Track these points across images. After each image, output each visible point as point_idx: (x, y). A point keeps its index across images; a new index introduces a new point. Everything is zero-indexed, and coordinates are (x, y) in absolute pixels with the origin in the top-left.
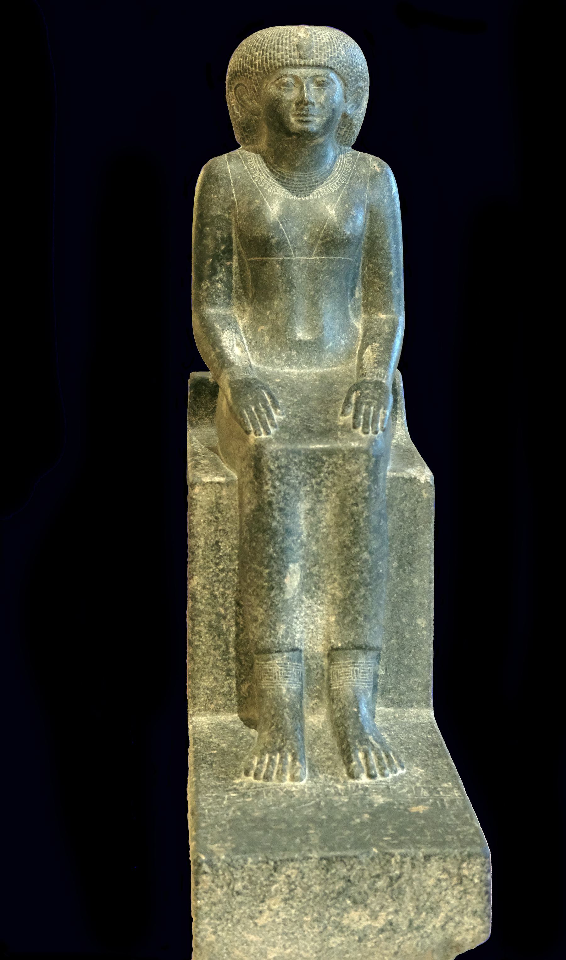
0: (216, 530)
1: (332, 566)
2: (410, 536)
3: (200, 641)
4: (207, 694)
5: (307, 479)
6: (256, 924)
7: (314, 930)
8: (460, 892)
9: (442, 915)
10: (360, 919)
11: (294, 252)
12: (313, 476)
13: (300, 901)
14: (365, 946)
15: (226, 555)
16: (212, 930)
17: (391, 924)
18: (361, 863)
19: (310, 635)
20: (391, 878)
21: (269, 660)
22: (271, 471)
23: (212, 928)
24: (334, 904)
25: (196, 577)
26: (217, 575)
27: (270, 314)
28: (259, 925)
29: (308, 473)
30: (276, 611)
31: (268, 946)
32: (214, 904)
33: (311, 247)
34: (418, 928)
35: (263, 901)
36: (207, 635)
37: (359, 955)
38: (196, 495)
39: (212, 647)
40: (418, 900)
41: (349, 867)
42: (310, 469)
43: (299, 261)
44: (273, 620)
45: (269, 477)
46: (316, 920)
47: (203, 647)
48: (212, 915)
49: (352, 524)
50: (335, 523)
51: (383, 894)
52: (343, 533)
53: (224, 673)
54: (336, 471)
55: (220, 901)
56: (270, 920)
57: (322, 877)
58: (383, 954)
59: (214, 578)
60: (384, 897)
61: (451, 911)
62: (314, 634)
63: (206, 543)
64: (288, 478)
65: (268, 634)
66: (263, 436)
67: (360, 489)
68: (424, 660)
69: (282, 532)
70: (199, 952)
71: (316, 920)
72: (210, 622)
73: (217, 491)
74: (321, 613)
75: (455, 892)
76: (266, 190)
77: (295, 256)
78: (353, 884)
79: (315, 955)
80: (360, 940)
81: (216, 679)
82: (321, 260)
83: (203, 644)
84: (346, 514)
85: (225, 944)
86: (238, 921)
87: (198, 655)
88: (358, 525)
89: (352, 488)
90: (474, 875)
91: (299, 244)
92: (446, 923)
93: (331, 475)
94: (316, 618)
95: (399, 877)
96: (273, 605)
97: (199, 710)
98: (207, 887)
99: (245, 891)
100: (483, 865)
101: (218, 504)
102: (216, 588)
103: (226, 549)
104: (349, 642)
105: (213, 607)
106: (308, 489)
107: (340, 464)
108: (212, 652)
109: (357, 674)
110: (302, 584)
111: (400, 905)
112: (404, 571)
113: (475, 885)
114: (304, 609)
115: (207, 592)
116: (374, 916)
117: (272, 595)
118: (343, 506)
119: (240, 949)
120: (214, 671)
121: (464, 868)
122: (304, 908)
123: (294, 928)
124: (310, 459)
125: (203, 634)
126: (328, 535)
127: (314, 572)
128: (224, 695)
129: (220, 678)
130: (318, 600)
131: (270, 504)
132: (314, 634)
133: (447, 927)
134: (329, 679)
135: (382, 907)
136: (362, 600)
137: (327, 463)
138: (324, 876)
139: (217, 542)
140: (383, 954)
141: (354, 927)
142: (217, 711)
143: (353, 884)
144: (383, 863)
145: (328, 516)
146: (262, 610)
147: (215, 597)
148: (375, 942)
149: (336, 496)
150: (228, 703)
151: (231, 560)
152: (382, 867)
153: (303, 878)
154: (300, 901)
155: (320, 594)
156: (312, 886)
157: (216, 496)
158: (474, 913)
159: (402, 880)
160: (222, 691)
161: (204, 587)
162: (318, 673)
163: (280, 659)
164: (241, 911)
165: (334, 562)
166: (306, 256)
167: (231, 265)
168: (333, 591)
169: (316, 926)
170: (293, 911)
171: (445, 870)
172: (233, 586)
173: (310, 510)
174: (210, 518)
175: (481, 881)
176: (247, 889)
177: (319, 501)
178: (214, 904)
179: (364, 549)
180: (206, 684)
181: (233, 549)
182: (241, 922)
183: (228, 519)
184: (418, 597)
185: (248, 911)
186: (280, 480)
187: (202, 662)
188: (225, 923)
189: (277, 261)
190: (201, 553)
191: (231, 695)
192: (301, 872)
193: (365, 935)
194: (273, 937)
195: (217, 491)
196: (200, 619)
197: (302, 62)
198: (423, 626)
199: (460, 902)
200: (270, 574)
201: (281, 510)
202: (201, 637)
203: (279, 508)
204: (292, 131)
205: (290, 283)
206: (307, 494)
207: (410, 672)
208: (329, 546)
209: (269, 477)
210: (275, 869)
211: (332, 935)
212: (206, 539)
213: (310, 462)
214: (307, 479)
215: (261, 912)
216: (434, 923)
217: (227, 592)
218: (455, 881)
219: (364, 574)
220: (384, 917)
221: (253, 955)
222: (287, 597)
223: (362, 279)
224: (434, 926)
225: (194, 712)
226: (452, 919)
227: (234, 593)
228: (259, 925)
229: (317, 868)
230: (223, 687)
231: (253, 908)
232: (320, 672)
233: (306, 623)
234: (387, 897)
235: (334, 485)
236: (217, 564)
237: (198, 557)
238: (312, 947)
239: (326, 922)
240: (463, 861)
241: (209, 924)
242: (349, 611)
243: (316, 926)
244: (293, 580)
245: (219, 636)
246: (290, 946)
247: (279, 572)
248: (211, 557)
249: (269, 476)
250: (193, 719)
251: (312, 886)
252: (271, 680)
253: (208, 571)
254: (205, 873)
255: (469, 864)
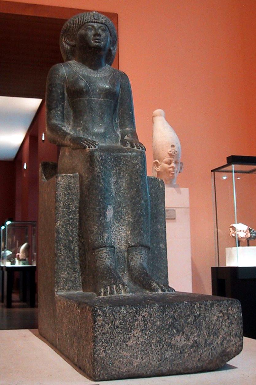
0: (68, 199)
1: (127, 208)
2: (155, 205)
3: (61, 254)
4: (64, 281)
5: (114, 167)
6: (127, 345)
7: (157, 348)
8: (229, 323)
9: (221, 336)
10: (181, 340)
11: (93, 96)
12: (116, 166)
13: (150, 331)
14: (184, 356)
15: (73, 211)
16: (103, 350)
17: (196, 343)
18: (180, 308)
19: (118, 241)
20: (195, 316)
21: (101, 251)
22: (98, 161)
23: (103, 348)
24: (167, 332)
25: (59, 221)
26: (69, 221)
27: (83, 122)
28: (129, 346)
29: (115, 164)
30: (103, 227)
31: (133, 358)
32: (104, 334)
33: (100, 94)
34: (210, 344)
35: (130, 332)
36: (64, 251)
37: (181, 361)
38: (59, 181)
39: (66, 257)
40: (209, 328)
41: (174, 310)
42: (115, 162)
43: (95, 100)
44: (102, 231)
45: (97, 164)
46: (159, 342)
47: (62, 257)
48: (103, 341)
49: (135, 188)
50: (128, 188)
51: (192, 326)
52: (132, 192)
53: (72, 270)
54: (127, 164)
55: (108, 332)
56: (134, 342)
57: (161, 316)
58: (193, 361)
59: (68, 222)
60: (192, 327)
61: (225, 334)
62: (120, 240)
63: (63, 205)
64: (106, 165)
65: (99, 238)
66: (93, 148)
67: (139, 171)
68: (164, 264)
69: (104, 190)
70: (96, 364)
71: (159, 342)
72: (66, 244)
73: (69, 180)
74: (123, 230)
75: (226, 324)
76: (80, 73)
77: (93, 98)
78: (176, 320)
79: (158, 363)
80: (181, 353)
81: (68, 273)
82: (104, 100)
83: (62, 255)
84: (133, 183)
85: (111, 358)
86: (118, 344)
87: (60, 261)
88: (138, 188)
89: (135, 171)
90: (234, 314)
91: (95, 93)
92: (223, 341)
93: (125, 166)
94: (121, 233)
95: (199, 315)
96: (101, 224)
97: (60, 289)
98: (100, 324)
99: (121, 326)
100: (238, 308)
101: (69, 186)
102: (68, 227)
103: (73, 208)
104: (137, 242)
105: (67, 236)
106: (115, 172)
107: (129, 160)
108: (66, 259)
109: (142, 257)
110: (114, 216)
111: (200, 332)
112: (153, 221)
113: (236, 319)
114: (115, 228)
115: (64, 229)
116: (188, 339)
117: (101, 219)
118: (131, 179)
119: (118, 361)
120: (67, 269)
121: (230, 310)
122: (152, 335)
123: (147, 347)
124: (115, 157)
125: (62, 250)
126: (124, 193)
127: (119, 211)
128: (72, 281)
129: (70, 273)
130: (121, 224)
131: (98, 176)
132: (120, 240)
133: (223, 343)
134: (128, 262)
135: (191, 333)
136: (142, 223)
137: (123, 160)
138: (162, 316)
139: (69, 205)
140: (193, 361)
141: (178, 345)
142: (69, 290)
143: (176, 320)
144: (191, 308)
145: (124, 185)
146: (96, 227)
147: (68, 231)
148: (189, 354)
149: (128, 175)
150: (74, 286)
151: (75, 214)
152: (191, 311)
153: (151, 317)
154: (150, 331)
155: (122, 221)
156: (156, 322)
157: (68, 182)
158: (236, 335)
159: (201, 317)
160: (71, 279)
161: (63, 227)
162: (122, 260)
163: (106, 250)
164: (119, 338)
165: (128, 205)
166: (98, 98)
167: (64, 105)
168: (128, 219)
169: (158, 346)
170: (146, 337)
171: (221, 312)
172: (76, 227)
173: (115, 182)
174: (66, 193)
175: (238, 317)
176: (122, 325)
177: (120, 178)
178: (104, 334)
179: (142, 199)
180: (63, 276)
181: (76, 209)
182: (119, 344)
183: (74, 193)
184: (160, 234)
185: (122, 337)
186: (102, 166)
187: (62, 265)
188: (110, 345)
189: (86, 99)
190: (61, 210)
191: (75, 282)
192: (150, 314)
193: (184, 350)
194: (136, 353)
195: (69, 180)
196: (61, 242)
197: (96, 21)
198: (163, 247)
199: (229, 329)
200: (100, 209)
201: (103, 179)
202: (61, 251)
203: (102, 178)
204: (92, 46)
205: (91, 109)
206: (114, 174)
207: (158, 270)
208: (126, 199)
209: (97, 164)
210: (136, 312)
211: (167, 350)
212: (63, 203)
213: (115, 159)
214: (114, 167)
215: (129, 338)
216: (217, 341)
217: (73, 229)
218: (226, 317)
219: (143, 211)
220: (192, 339)
221: (125, 364)
222: (108, 220)
223: (119, 115)
224: (217, 343)
225: (58, 290)
226: (226, 339)
227: (77, 230)
228: (129, 346)
229: (158, 311)
230: (72, 277)
231: (125, 336)
232: (124, 259)
233: (116, 235)
234: (194, 327)
235: (126, 170)
236: (69, 215)
237: (60, 211)
238: (156, 358)
239: (164, 343)
240: (229, 306)
241: (102, 346)
242: (137, 228)
243: (158, 346)
244: (110, 213)
245: (70, 251)
246: (145, 358)
247: (103, 208)
248: (66, 212)
249: (97, 163)
250: (58, 293)
251: (156, 322)
252: (102, 260)
253: (64, 218)
254: (100, 315)
255: (231, 308)
